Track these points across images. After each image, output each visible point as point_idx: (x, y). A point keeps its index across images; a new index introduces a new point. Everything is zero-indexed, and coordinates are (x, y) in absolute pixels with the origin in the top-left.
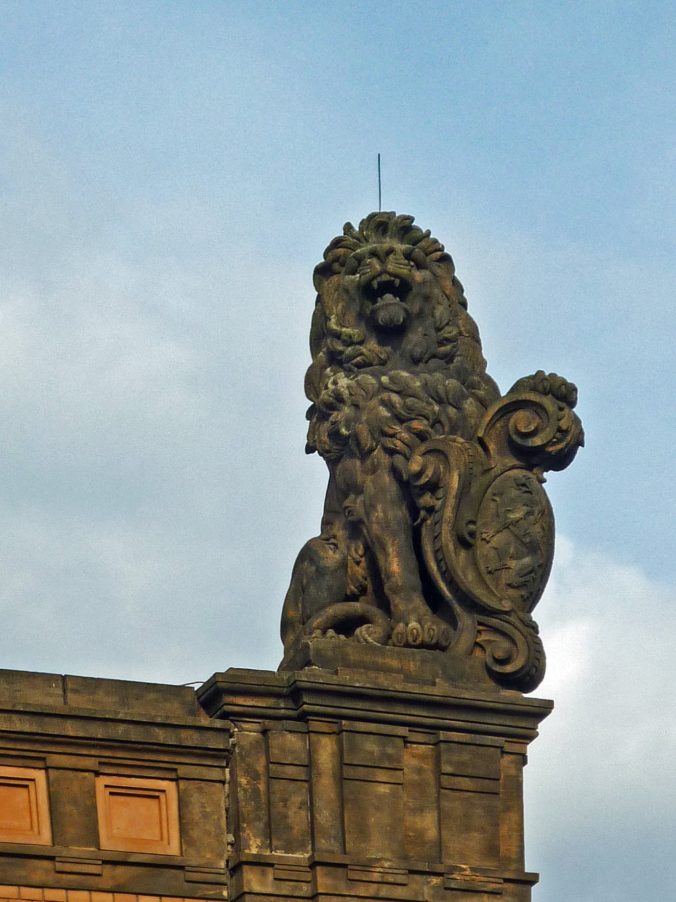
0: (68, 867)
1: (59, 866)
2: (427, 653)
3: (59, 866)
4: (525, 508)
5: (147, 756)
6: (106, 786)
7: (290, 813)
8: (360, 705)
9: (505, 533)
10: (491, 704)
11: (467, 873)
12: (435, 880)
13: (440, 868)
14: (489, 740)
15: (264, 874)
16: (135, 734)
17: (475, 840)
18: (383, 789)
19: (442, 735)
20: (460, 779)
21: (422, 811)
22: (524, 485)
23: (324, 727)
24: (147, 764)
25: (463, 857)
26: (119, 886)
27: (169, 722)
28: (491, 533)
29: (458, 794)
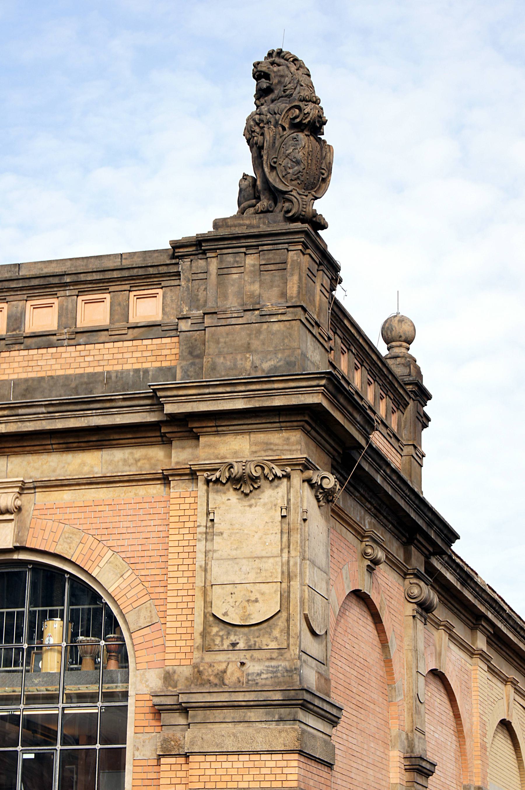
0: (113, 333)
1: (110, 333)
2: (262, 215)
3: (110, 333)
4: (293, 148)
5: (148, 280)
6: (135, 296)
7: (200, 294)
8: (226, 242)
9: (287, 159)
10: (280, 231)
11: (269, 307)
12: (257, 312)
13: (257, 307)
14: (280, 246)
15: (187, 322)
16: (141, 272)
17: (275, 291)
18: (236, 276)
19: (261, 248)
20: (269, 266)
21: (254, 282)
22: (295, 138)
23: (213, 255)
24: (149, 283)
25: (269, 300)
26: (134, 337)
27: (153, 264)
28: (282, 160)
29: (268, 272)
